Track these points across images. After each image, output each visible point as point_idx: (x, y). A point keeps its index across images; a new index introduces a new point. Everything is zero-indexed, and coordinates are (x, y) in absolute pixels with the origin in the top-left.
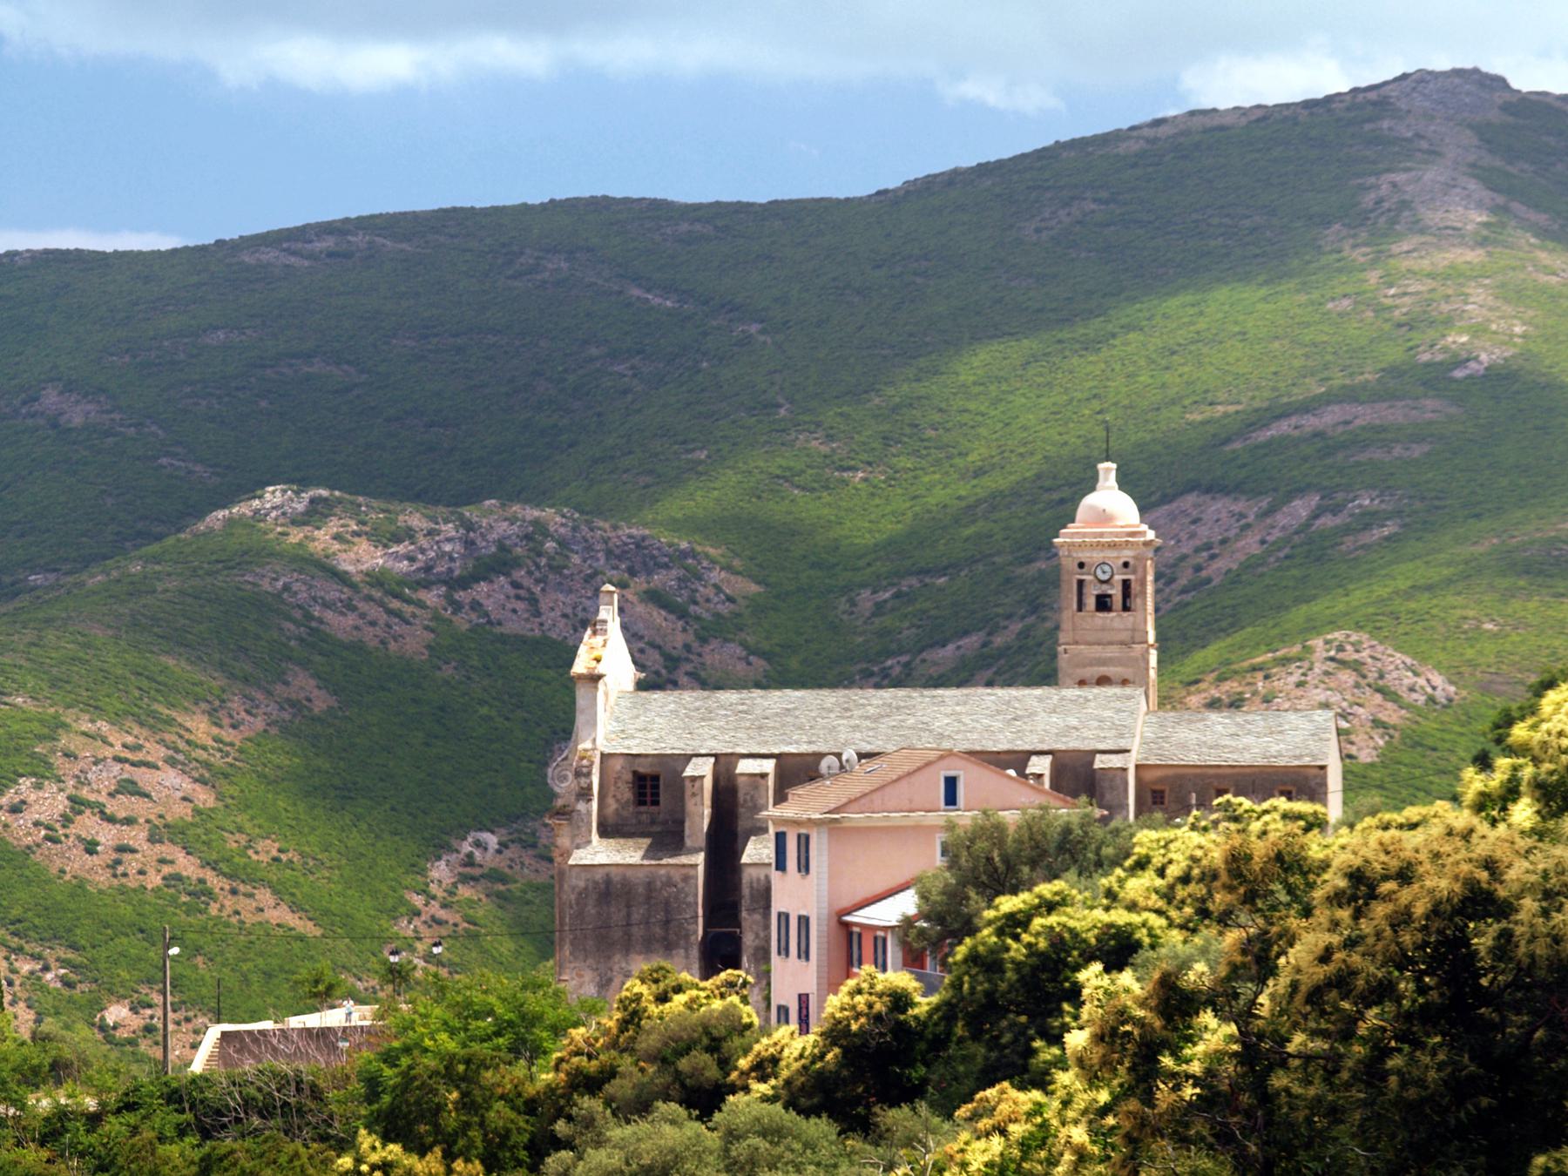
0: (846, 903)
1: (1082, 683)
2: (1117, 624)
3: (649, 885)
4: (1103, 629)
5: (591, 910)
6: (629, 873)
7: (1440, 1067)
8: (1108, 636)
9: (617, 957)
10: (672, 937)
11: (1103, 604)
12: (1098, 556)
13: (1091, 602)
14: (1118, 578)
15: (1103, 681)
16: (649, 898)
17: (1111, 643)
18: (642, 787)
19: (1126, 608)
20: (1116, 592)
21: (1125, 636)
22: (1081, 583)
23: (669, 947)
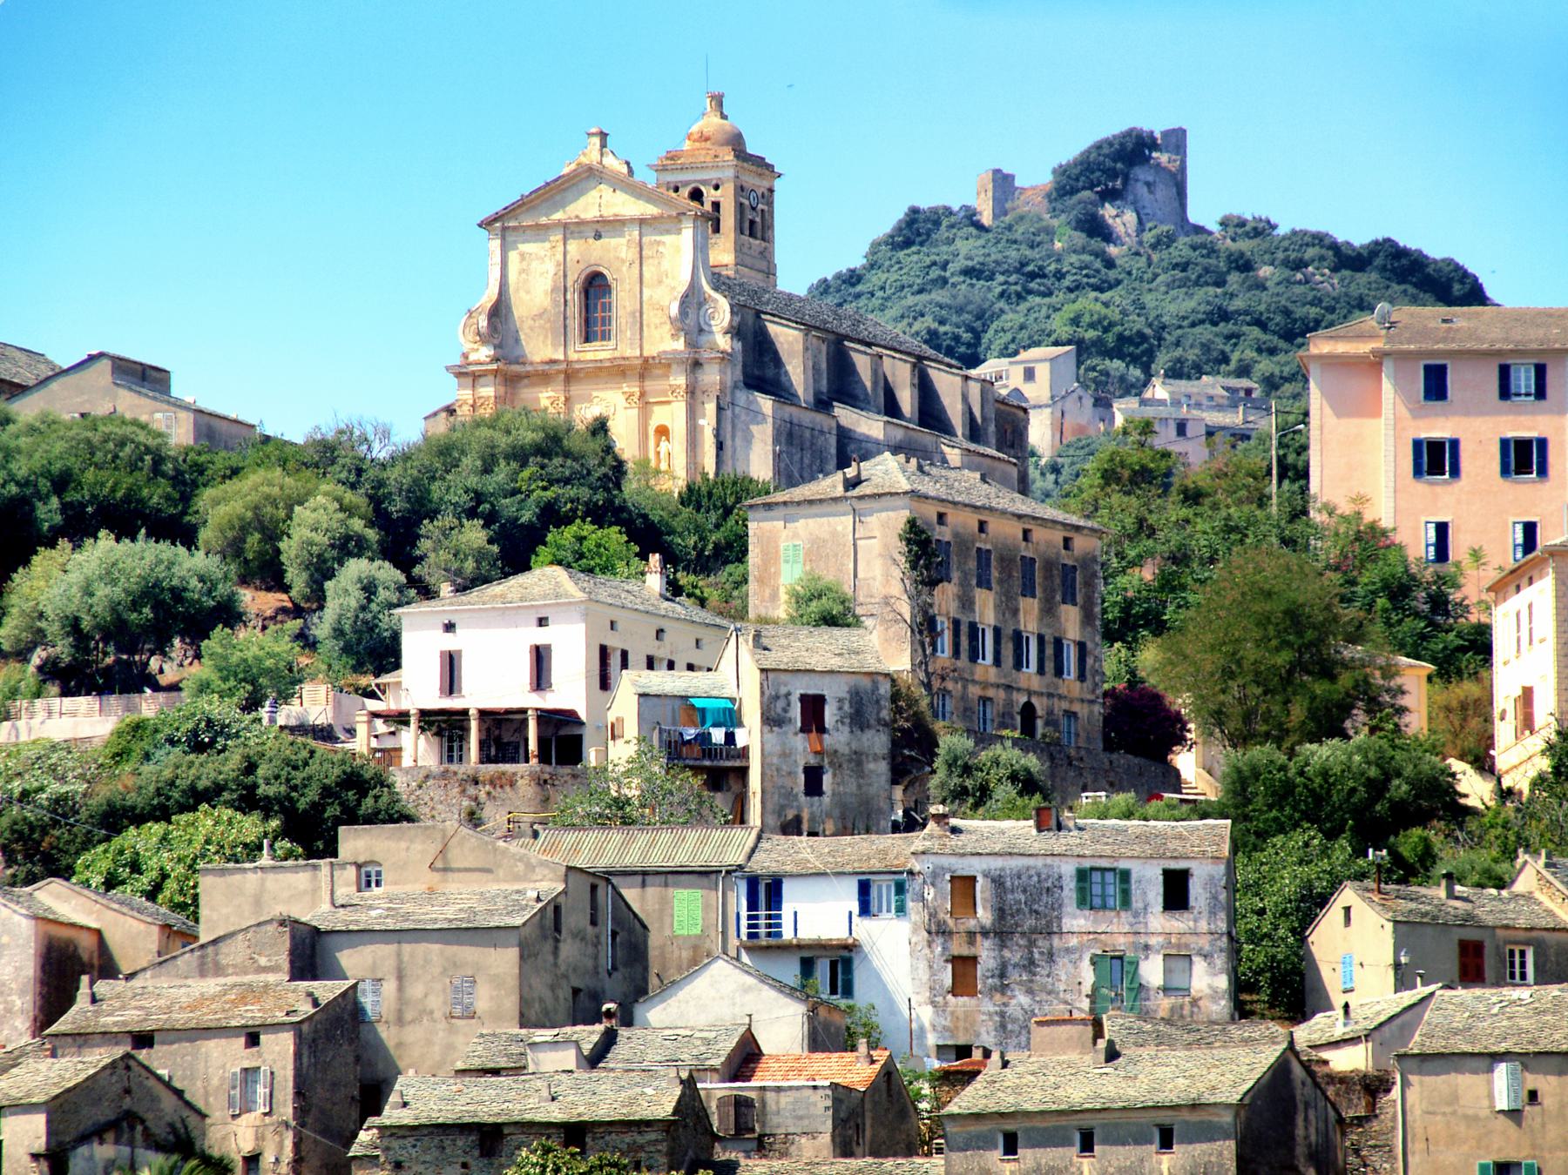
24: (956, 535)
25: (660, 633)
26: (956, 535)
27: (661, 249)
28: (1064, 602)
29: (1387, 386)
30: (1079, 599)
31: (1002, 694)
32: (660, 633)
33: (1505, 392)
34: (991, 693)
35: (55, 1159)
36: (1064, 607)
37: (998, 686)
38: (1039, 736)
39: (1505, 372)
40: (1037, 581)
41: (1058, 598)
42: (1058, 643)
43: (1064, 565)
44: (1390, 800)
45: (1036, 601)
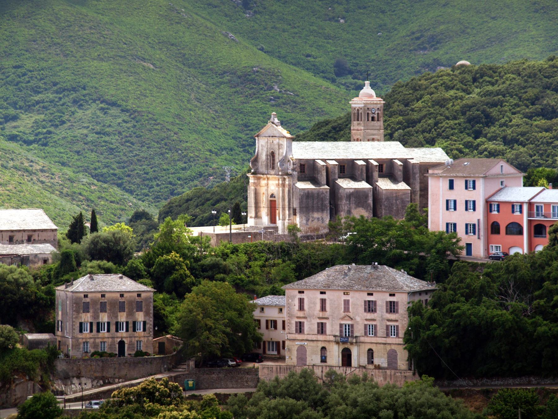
0: (487, 197)
1: (369, 140)
2: (376, 125)
3: (318, 194)
4: (373, 126)
5: (304, 200)
6: (313, 191)
7: (180, 257)
8: (374, 128)
9: (311, 213)
10: (323, 208)
11: (373, 119)
12: (372, 106)
13: (370, 119)
14: (377, 112)
15: (373, 140)
16: (318, 197)
17: (375, 130)
18: (341, 168)
19: (378, 120)
20: (376, 116)
21: (378, 128)
22: (368, 113)
23: (323, 210)
24: (92, 300)
25: (502, 182)
26: (92, 300)
28: (137, 311)
29: (441, 184)
30: (144, 309)
31: (110, 340)
32: (502, 182)
33: (466, 188)
34: (105, 340)
35: (122, 418)
36: (137, 313)
37: (108, 338)
38: (126, 354)
39: (466, 182)
40: (126, 307)
41: (135, 310)
42: (134, 323)
43: (137, 302)
44: (443, 415)
45: (125, 313)
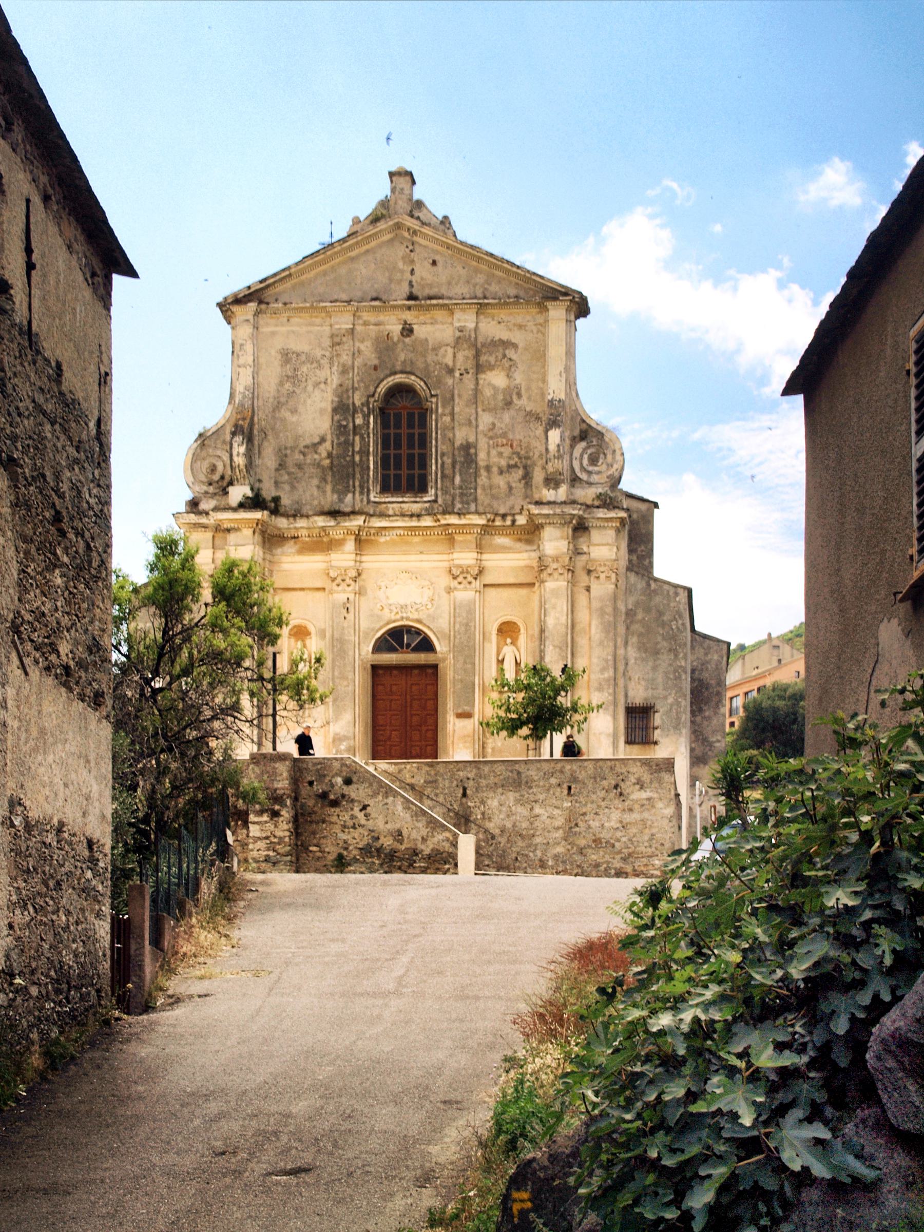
27: (510, 353)
